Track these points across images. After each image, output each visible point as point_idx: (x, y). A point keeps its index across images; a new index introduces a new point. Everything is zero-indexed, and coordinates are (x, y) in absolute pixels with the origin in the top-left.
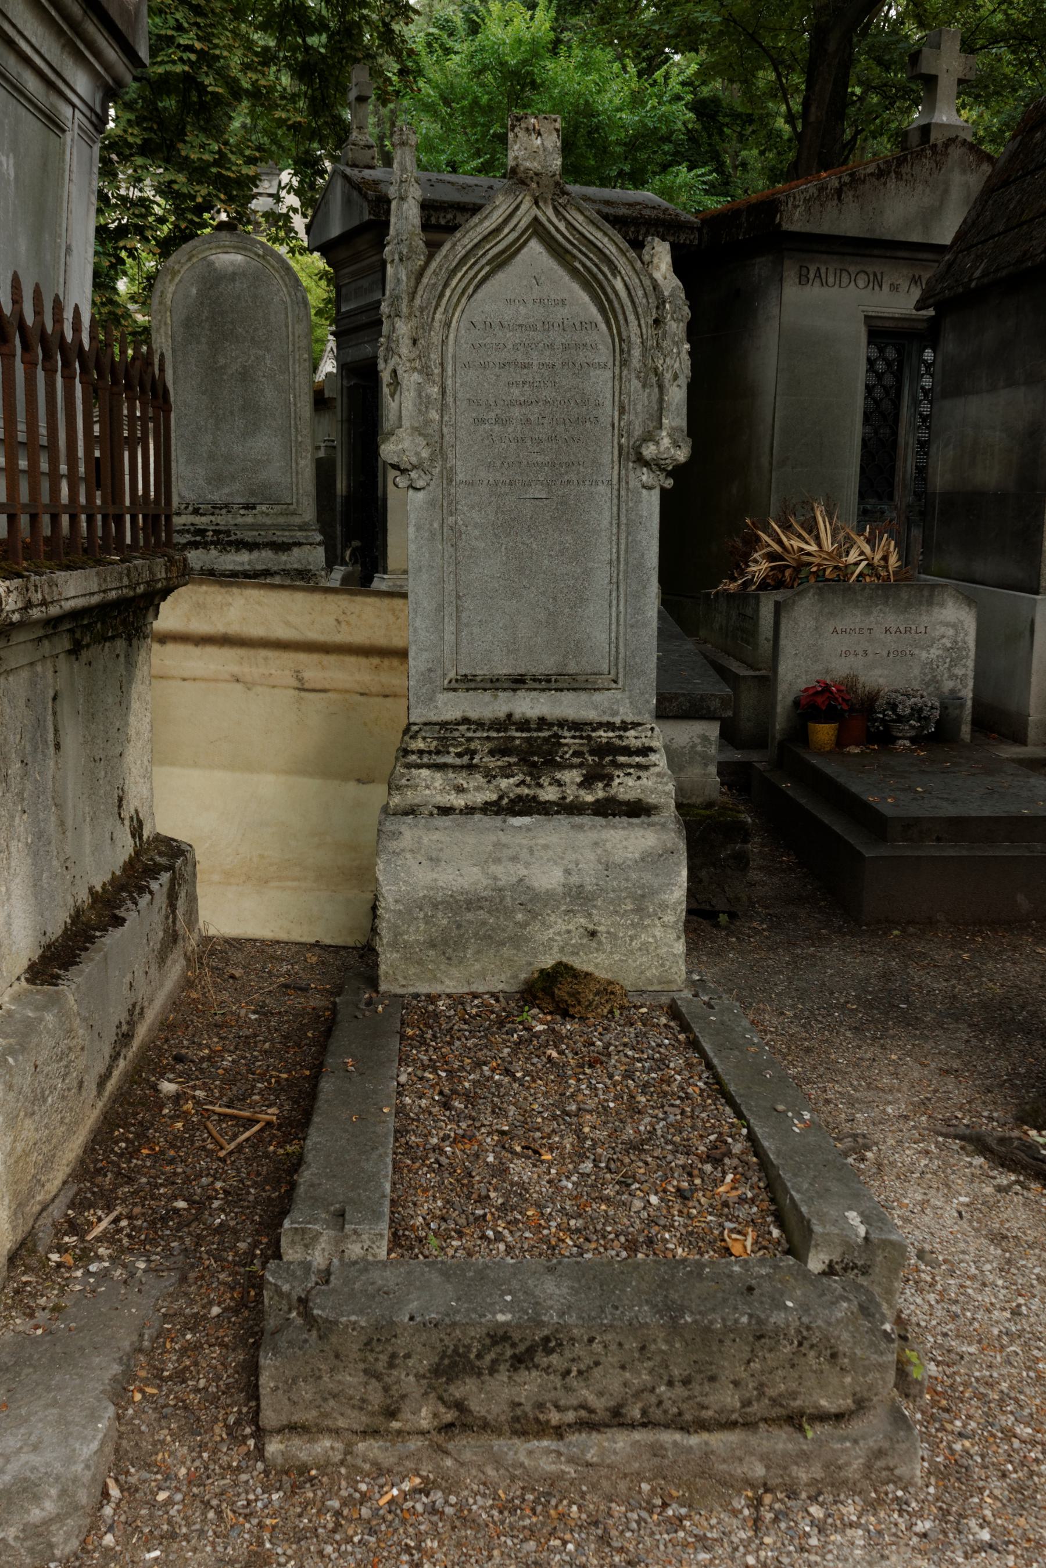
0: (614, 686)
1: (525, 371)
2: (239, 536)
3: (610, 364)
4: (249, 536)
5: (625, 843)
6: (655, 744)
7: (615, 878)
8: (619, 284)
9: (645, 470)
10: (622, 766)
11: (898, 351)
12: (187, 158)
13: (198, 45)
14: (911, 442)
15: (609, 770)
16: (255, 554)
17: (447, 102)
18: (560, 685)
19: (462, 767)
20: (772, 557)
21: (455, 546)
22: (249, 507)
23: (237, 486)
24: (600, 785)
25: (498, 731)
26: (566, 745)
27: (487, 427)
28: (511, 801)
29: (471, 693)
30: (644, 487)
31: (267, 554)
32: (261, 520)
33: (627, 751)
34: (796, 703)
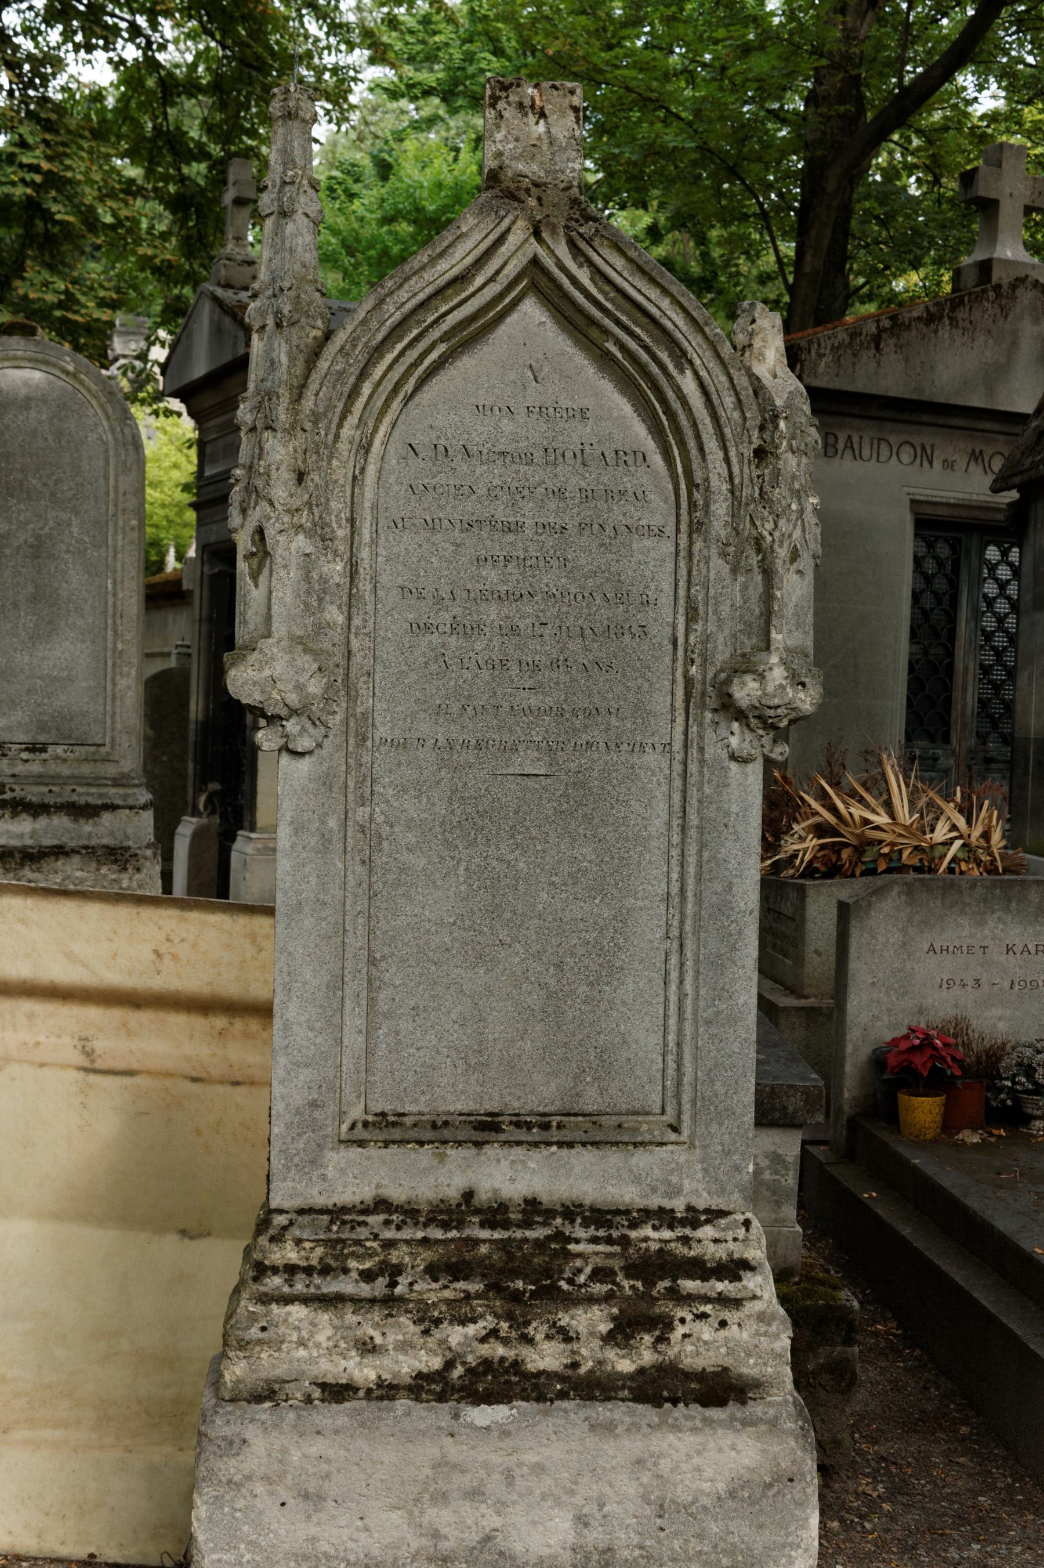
0: (673, 1137)
1: (510, 537)
2: (18, 794)
3: (670, 529)
4: (33, 793)
5: (696, 1461)
6: (756, 1253)
7: (677, 1534)
8: (688, 384)
9: (735, 726)
10: (689, 1299)
11: (953, 548)
12: (25, 297)
13: (45, 165)
14: (971, 666)
15: (664, 1307)
16: (43, 822)
17: (351, 253)
18: (567, 1135)
19: (373, 1301)
20: (820, 830)
21: (368, 863)
22: (34, 748)
23: (18, 716)
24: (648, 1339)
25: (446, 1226)
26: (579, 1255)
27: (435, 639)
28: (470, 1371)
29: (393, 1149)
30: (733, 757)
31: (61, 822)
32: (54, 768)
33: (699, 1268)
34: (878, 1061)
